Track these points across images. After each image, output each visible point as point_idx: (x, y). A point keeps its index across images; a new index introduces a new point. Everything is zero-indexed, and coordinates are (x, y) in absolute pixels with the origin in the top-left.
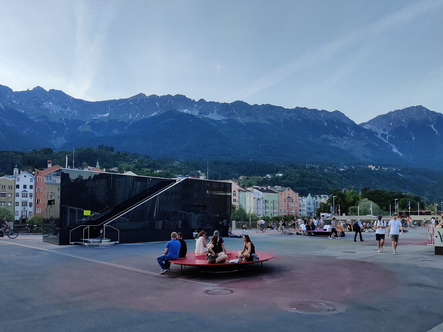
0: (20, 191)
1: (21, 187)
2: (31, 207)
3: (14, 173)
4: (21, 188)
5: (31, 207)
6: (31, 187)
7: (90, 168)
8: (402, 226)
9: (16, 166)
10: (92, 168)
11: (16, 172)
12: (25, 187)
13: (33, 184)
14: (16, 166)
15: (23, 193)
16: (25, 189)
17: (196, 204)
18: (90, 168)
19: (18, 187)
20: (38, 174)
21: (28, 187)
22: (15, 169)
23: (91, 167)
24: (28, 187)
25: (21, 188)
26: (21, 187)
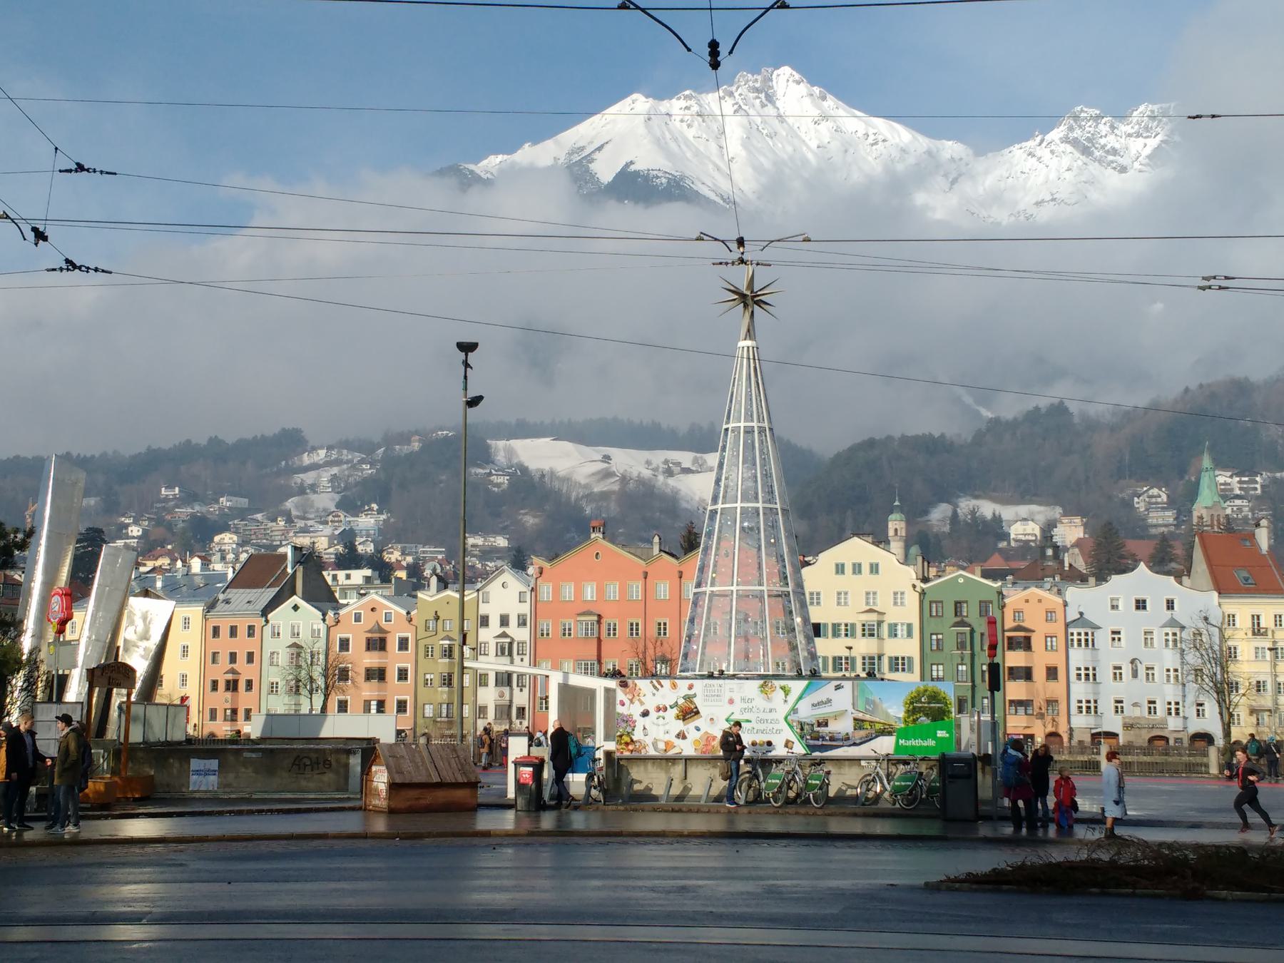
0: (488, 635)
1: (494, 621)
2: (524, 689)
3: (891, 533)
4: (495, 627)
5: (524, 689)
6: (522, 623)
7: (1229, 480)
8: (431, 737)
9: (897, 503)
10: (1238, 479)
11: (896, 530)
12: (504, 621)
13: (525, 609)
14: (897, 503)
15: (497, 643)
16: (503, 629)
17: (762, 672)
18: (1229, 480)
19: (484, 621)
20: (541, 573)
21: (513, 621)
22: (892, 517)
23: (1231, 477)
24: (513, 621)
25: (495, 627)
26: (494, 621)
